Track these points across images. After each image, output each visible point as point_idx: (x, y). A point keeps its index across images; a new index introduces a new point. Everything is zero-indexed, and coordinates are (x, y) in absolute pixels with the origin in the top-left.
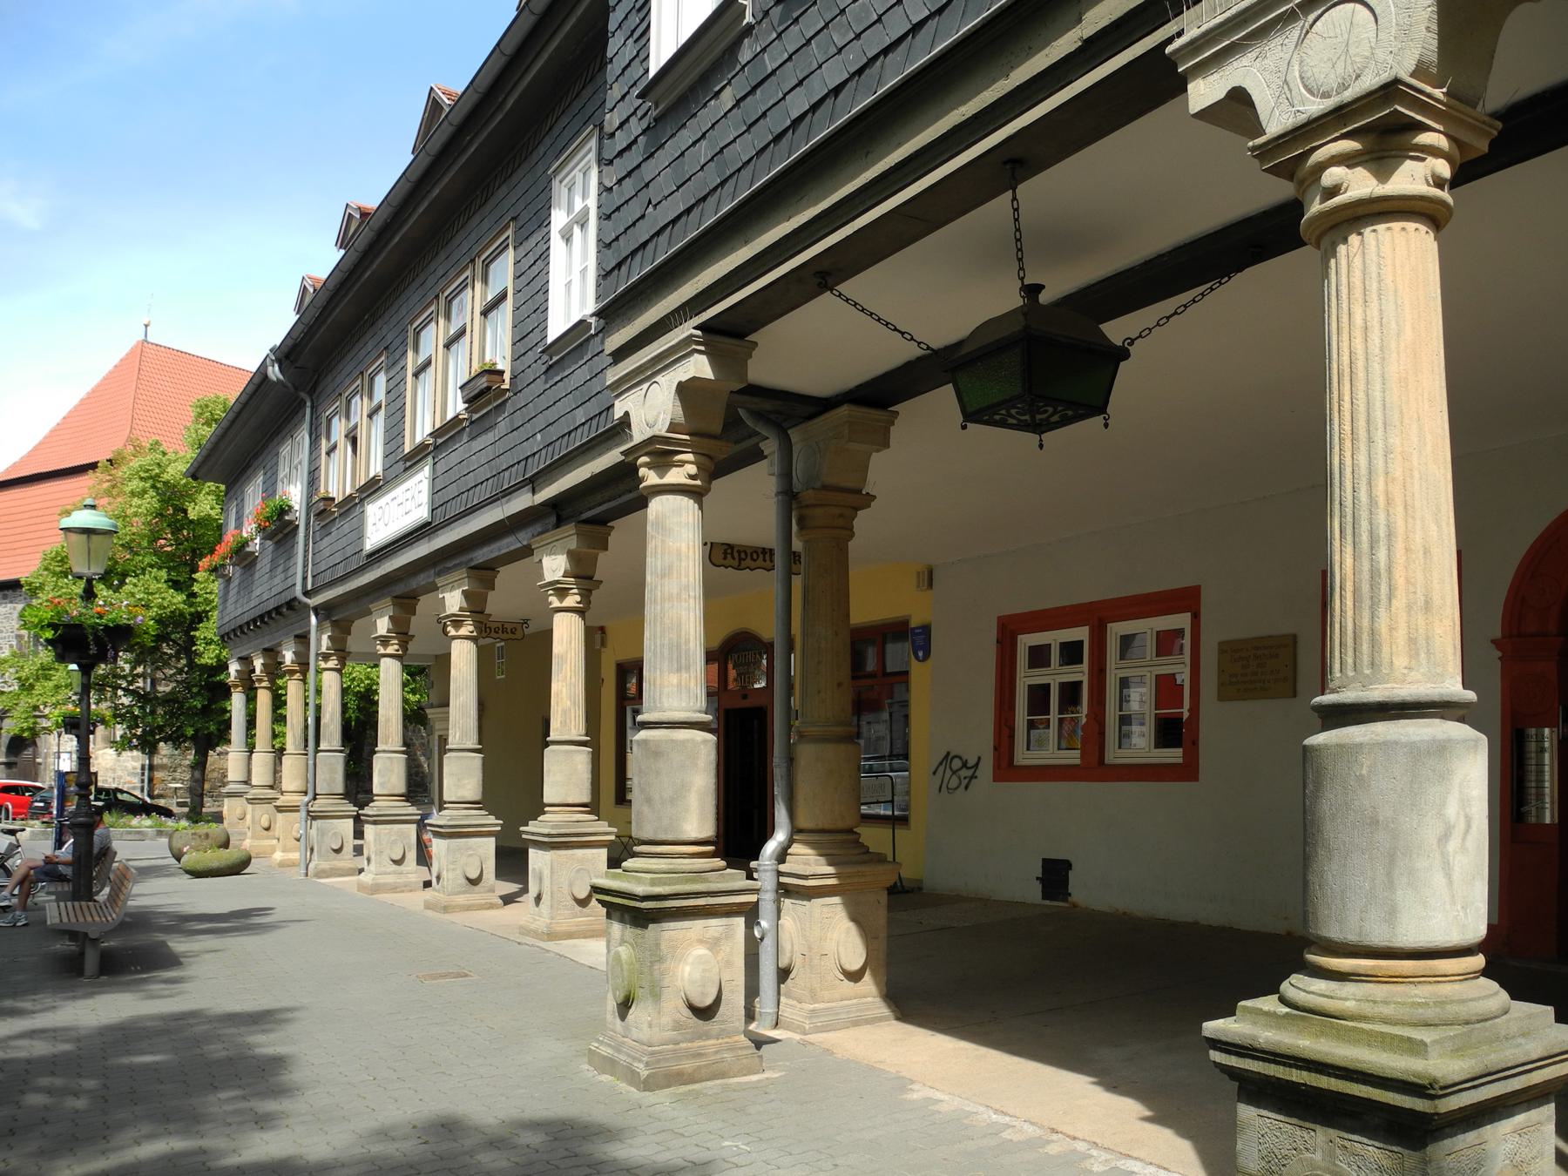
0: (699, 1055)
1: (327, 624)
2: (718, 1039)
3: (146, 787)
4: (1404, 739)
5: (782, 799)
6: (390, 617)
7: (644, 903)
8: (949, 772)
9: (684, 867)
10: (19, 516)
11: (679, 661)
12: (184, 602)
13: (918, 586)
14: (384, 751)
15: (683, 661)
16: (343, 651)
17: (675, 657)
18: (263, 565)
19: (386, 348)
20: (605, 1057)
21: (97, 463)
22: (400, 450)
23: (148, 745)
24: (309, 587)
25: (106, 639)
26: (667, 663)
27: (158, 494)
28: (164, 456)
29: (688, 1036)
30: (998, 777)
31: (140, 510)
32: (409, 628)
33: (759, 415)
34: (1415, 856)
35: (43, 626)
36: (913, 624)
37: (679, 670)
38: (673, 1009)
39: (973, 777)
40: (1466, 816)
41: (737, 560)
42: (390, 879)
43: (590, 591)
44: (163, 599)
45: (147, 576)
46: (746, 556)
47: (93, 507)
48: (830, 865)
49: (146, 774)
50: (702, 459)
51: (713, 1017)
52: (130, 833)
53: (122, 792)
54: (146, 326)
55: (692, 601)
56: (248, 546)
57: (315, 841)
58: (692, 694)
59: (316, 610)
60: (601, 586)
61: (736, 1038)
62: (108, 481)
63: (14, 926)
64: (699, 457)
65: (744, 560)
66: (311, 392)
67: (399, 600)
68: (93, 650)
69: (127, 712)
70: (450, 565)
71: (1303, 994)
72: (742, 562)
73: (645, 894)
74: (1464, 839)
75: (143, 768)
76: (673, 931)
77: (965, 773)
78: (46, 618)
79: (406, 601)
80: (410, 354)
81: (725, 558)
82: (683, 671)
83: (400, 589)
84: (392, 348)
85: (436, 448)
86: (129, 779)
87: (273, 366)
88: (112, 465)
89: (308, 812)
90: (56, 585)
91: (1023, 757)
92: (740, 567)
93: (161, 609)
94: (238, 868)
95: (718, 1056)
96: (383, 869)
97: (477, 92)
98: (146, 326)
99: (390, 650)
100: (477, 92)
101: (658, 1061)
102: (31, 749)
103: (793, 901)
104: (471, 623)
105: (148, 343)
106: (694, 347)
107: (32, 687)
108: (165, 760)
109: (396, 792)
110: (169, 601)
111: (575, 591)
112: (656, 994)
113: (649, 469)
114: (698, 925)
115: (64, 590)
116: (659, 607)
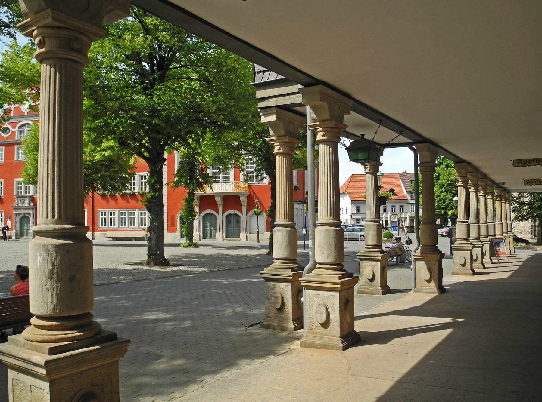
46: (527, 162)
65: (526, 163)
75: (532, 226)
81: (519, 164)
86: (528, 230)
99: (481, 194)
111: (461, 181)
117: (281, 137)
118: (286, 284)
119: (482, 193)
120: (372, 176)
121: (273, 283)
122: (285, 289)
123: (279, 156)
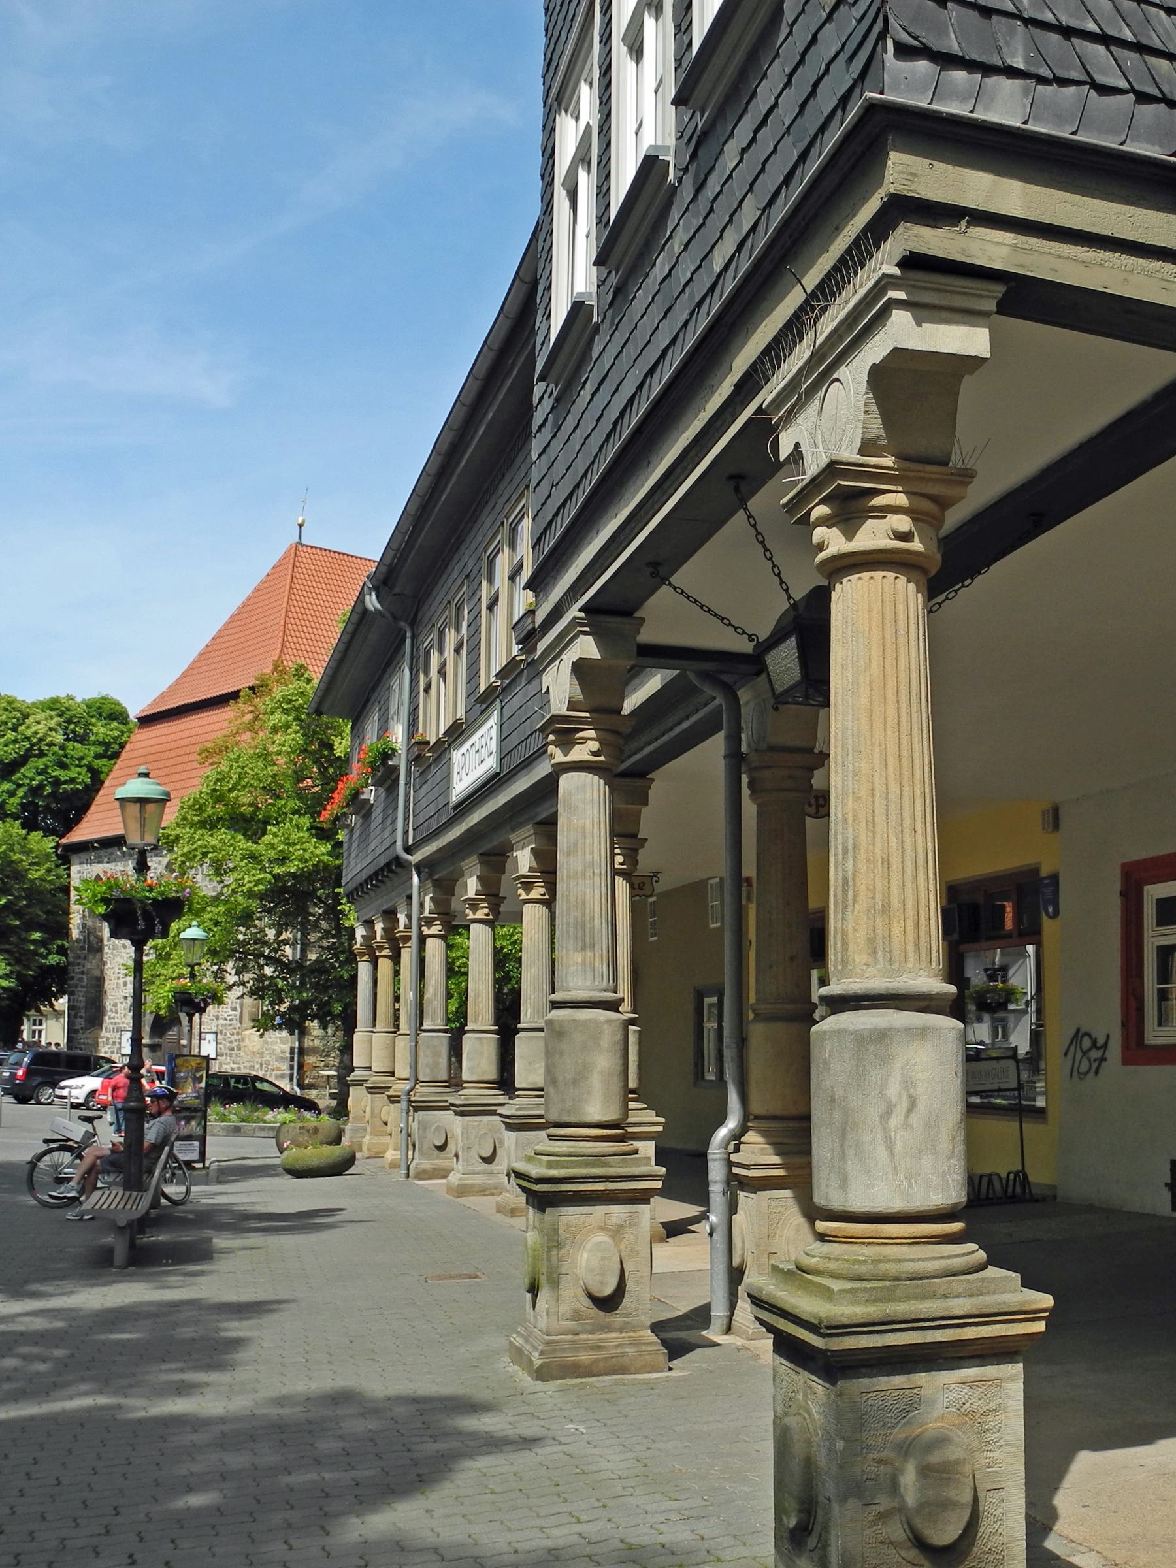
0: (599, 1348)
1: (429, 884)
2: (621, 1332)
3: (295, 1075)
4: (851, 1028)
5: (734, 1082)
6: (478, 877)
7: (538, 1186)
8: (1079, 1054)
9: (584, 1150)
10: (166, 755)
11: (584, 941)
12: (330, 854)
13: (1044, 829)
14: (473, 1031)
15: (587, 939)
16: (447, 914)
17: (579, 935)
18: (377, 814)
19: (467, 576)
20: (517, 1347)
21: (239, 691)
22: (477, 691)
23: (294, 1023)
24: (411, 842)
25: (154, 914)
26: (572, 942)
27: (302, 728)
28: (308, 684)
29: (589, 1327)
30: (1127, 1060)
31: (284, 749)
32: (500, 889)
33: (705, 676)
34: (860, 1130)
35: (96, 901)
36: (1044, 873)
37: (584, 948)
38: (572, 1298)
39: (1103, 1059)
40: (910, 1096)
41: (814, 806)
42: (478, 1180)
43: (636, 851)
44: (305, 850)
45: (288, 824)
47: (146, 775)
48: (777, 1154)
49: (296, 1059)
50: (604, 734)
51: (616, 1309)
52: (262, 1129)
53: (263, 1080)
54: (300, 526)
55: (597, 878)
56: (363, 793)
57: (416, 1136)
58: (597, 974)
59: (419, 867)
60: (646, 844)
61: (642, 1333)
62: (251, 712)
63: (81, 1219)
64: (600, 733)
66: (414, 623)
67: (486, 858)
68: (141, 925)
69: (270, 985)
70: (522, 819)
71: (912, 1264)
72: (820, 809)
73: (538, 1176)
74: (907, 1116)
75: (292, 1049)
76: (571, 1216)
77: (1095, 1054)
78: (100, 893)
79: (492, 858)
80: (484, 583)
82: (588, 949)
83: (487, 846)
84: (473, 575)
85: (503, 690)
86: (277, 1064)
87: (370, 594)
88: (254, 693)
89: (410, 1101)
90: (192, 838)
91: (1155, 1035)
92: (819, 815)
93: (302, 863)
94: (341, 1167)
95: (619, 1351)
96: (471, 1168)
97: (508, 318)
98: (300, 526)
99: (480, 914)
100: (508, 318)
101: (554, 1351)
102: (176, 1029)
103: (747, 1194)
104: (542, 884)
105: (303, 545)
106: (579, 629)
107: (168, 954)
108: (317, 1042)
109: (485, 1078)
110: (312, 852)
112: (555, 1283)
113: (556, 747)
114: (599, 1211)
115: (199, 843)
116: (565, 885)
117: (929, 468)
118: (991, 1371)
119: (486, 911)
120: (602, 782)
121: (898, 1380)
122: (978, 1404)
123: (891, 575)
